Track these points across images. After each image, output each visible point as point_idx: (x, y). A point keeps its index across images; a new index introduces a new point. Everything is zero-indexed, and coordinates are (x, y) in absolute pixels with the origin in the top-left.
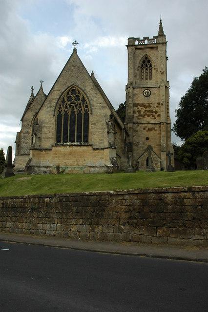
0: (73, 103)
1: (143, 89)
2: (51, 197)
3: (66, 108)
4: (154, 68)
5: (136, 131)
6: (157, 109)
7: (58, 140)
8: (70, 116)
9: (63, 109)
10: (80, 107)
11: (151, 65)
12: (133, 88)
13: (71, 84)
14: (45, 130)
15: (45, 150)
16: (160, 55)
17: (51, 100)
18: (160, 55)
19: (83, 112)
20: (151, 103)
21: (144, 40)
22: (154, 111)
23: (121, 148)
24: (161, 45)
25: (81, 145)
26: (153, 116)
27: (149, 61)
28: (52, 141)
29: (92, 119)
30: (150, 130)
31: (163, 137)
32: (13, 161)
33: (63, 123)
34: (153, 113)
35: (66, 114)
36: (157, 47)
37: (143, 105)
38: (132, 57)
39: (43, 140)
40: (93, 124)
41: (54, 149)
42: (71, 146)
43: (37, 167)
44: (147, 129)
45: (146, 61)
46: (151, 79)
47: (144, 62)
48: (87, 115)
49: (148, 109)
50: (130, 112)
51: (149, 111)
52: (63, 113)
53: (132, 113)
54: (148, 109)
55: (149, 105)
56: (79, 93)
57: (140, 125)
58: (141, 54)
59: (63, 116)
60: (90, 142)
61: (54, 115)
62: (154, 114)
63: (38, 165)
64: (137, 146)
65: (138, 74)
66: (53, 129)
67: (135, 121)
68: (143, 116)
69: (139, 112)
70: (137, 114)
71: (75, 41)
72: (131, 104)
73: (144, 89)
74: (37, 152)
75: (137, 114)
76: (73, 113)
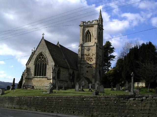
5: (81, 67)
6: (92, 57)
7: (35, 75)
17: (33, 58)
20: (89, 54)
29: (48, 67)
32: (23, 85)
33: (44, 66)
35: (38, 65)
40: (48, 69)
42: (43, 78)
44: (87, 67)
46: (90, 41)
48: (46, 65)
49: (88, 57)
54: (88, 57)
59: (37, 65)
64: (82, 75)
67: (82, 63)
74: (27, 80)
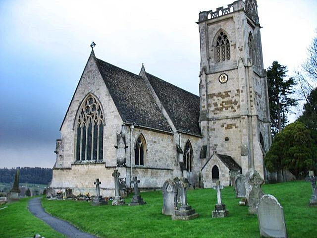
0: (91, 114)
1: (219, 74)
2: (69, 223)
3: (85, 120)
4: (231, 44)
6: (236, 98)
8: (88, 128)
9: (82, 121)
10: (96, 118)
11: (228, 41)
12: (207, 74)
13: (88, 92)
14: (67, 146)
15: (67, 169)
16: (237, 27)
17: (72, 113)
18: (237, 27)
19: (99, 124)
20: (230, 91)
21: (228, 9)
22: (233, 101)
23: (174, 158)
24: (237, 14)
25: (95, 163)
26: (232, 108)
27: (225, 37)
28: (72, 160)
30: (229, 127)
31: (244, 135)
34: (232, 104)
35: (84, 128)
36: (232, 18)
37: (220, 95)
38: (204, 34)
39: (65, 158)
41: (74, 167)
42: (87, 164)
43: (58, 188)
44: (225, 126)
45: (222, 37)
46: (229, 58)
47: (219, 38)
49: (226, 99)
50: (204, 107)
51: (227, 102)
52: (82, 126)
53: (206, 106)
54: (226, 99)
55: (227, 94)
56: (96, 102)
57: (217, 122)
58: (214, 30)
60: (104, 160)
61: (73, 130)
62: (233, 105)
63: (60, 187)
65: (213, 55)
66: (73, 145)
68: (221, 110)
69: (216, 104)
70: (213, 108)
71: (93, 43)
72: (204, 95)
73: (220, 74)
75: (213, 108)
76: (90, 125)
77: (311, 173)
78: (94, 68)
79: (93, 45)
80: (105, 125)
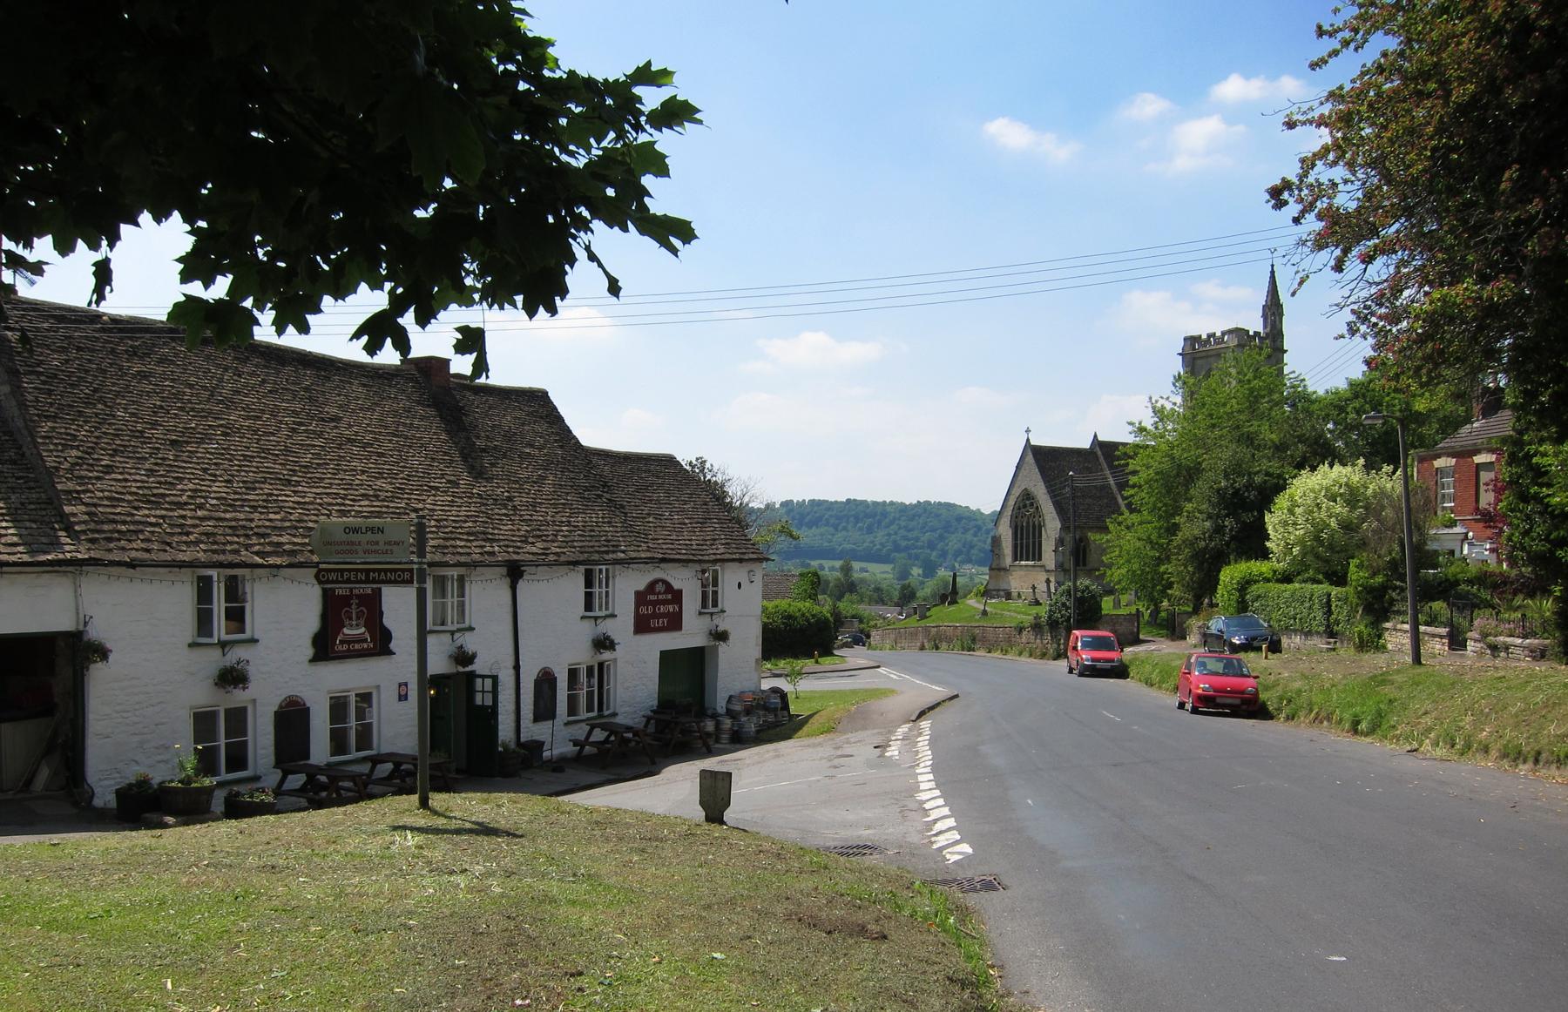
3: (1022, 517)
63: (997, 588)
76: (1028, 523)
77: (1552, 338)
78: (1030, 458)
79: (1028, 431)
80: (757, 637)
